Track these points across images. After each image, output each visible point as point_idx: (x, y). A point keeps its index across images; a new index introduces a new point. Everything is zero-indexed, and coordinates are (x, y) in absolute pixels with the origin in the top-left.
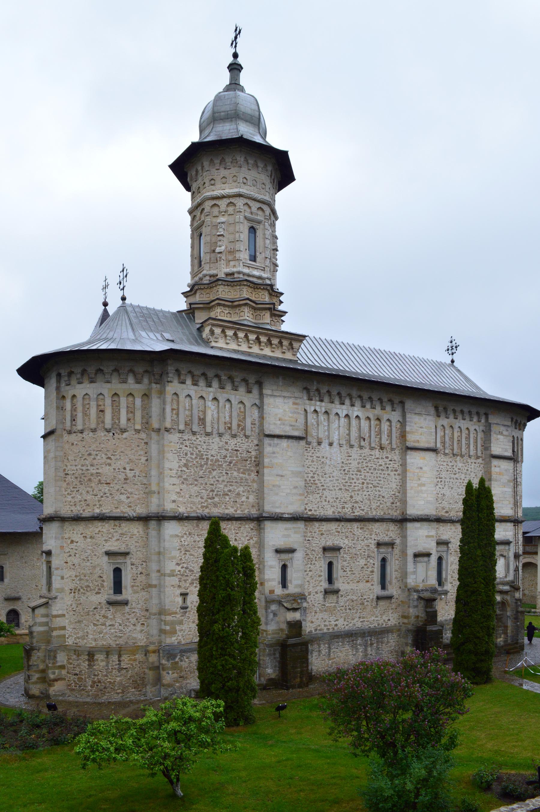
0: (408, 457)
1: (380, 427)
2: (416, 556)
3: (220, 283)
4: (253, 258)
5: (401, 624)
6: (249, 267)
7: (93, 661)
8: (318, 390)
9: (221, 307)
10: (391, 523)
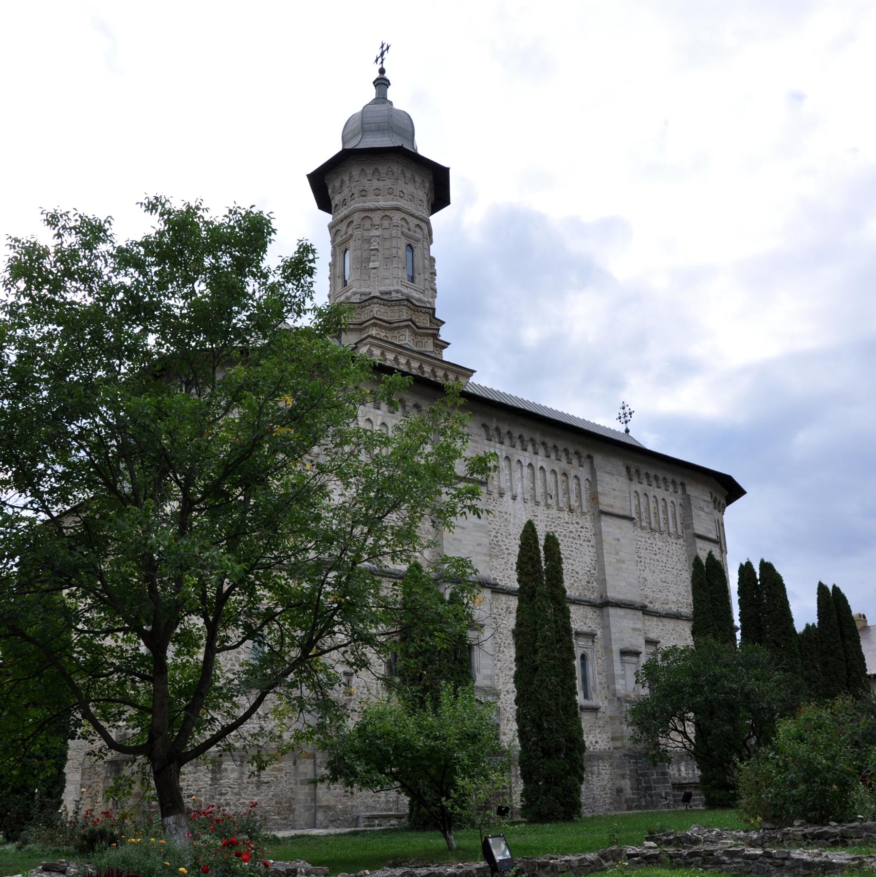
0: (602, 524)
1: (568, 485)
2: (624, 653)
3: (375, 301)
4: (412, 279)
5: (612, 749)
6: (407, 287)
7: (220, 772)
8: (497, 429)
9: (377, 328)
10: (589, 608)
